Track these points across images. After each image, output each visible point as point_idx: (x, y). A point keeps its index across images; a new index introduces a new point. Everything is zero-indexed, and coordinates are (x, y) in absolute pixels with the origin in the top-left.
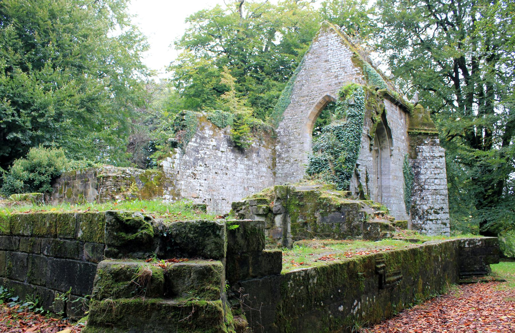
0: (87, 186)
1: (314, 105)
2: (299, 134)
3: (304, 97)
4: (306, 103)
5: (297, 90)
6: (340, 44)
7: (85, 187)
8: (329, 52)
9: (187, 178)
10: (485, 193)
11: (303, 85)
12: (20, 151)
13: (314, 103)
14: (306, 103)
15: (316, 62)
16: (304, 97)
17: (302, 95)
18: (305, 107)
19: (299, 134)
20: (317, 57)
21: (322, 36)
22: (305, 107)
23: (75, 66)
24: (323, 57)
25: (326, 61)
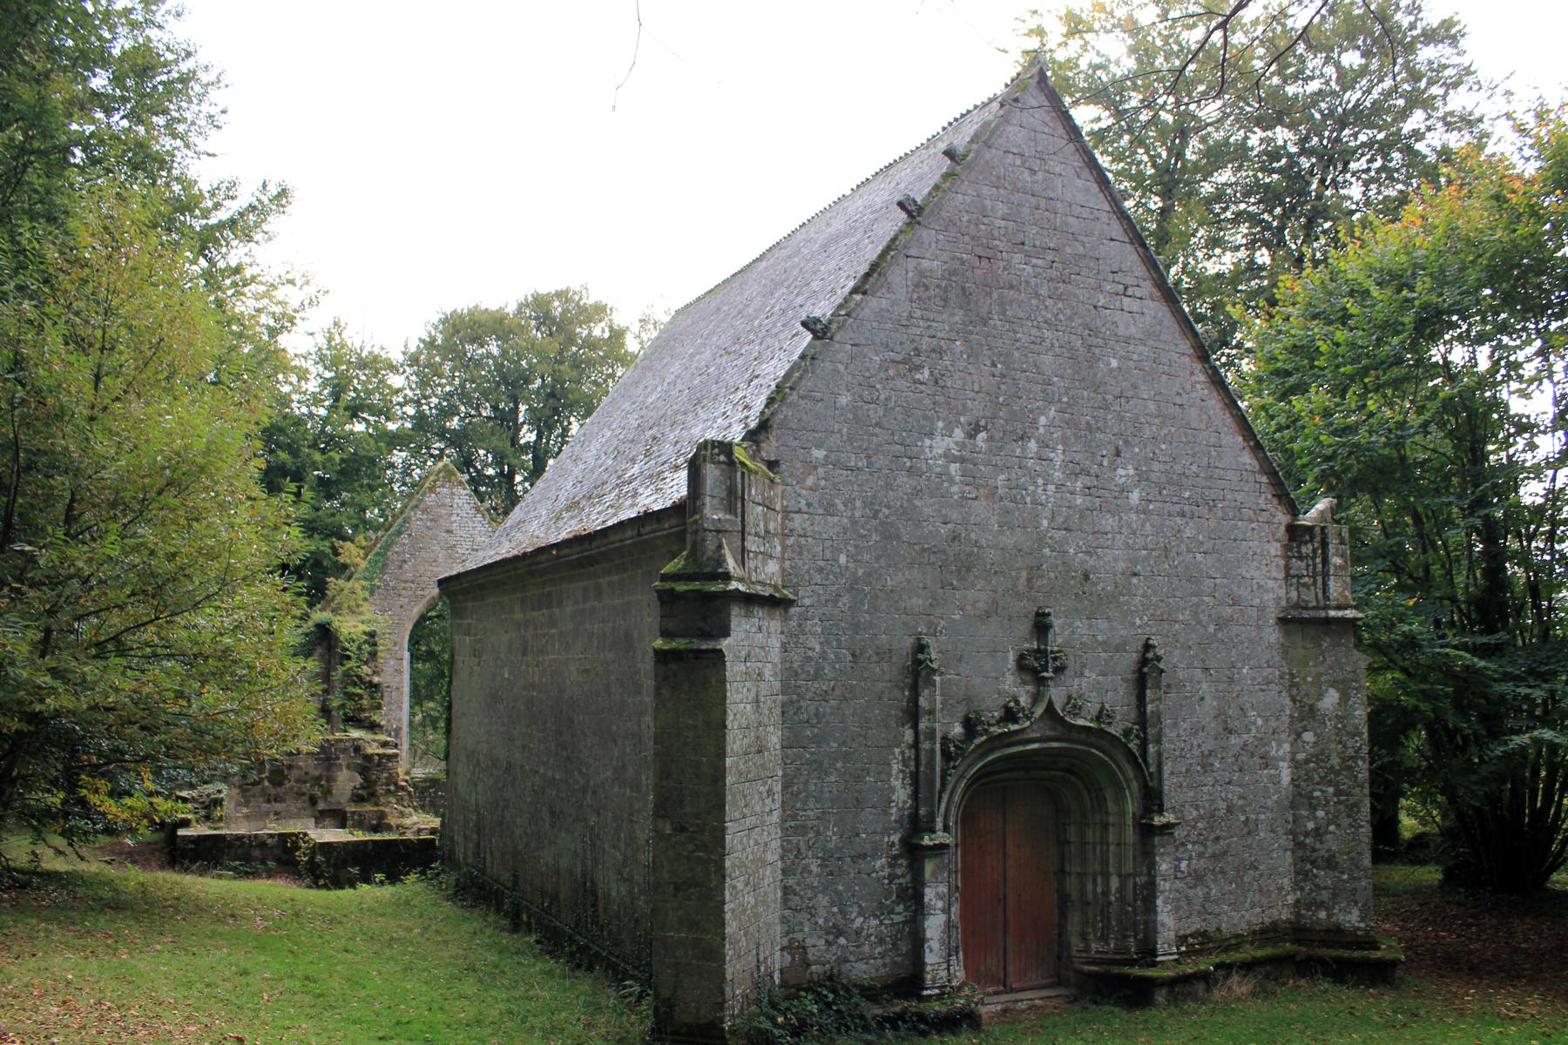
0: (334, 769)
1: (425, 601)
2: (395, 644)
3: (406, 582)
4: (410, 593)
5: (392, 568)
6: (473, 511)
7: (329, 768)
8: (454, 518)
9: (1463, 262)
10: (923, 482)
11: (405, 562)
12: (74, 156)
13: (423, 596)
14: (410, 593)
15: (429, 528)
16: (406, 582)
17: (403, 578)
18: (406, 600)
19: (395, 644)
20: (432, 520)
21: (443, 486)
22: (406, 600)
23: (915, 699)
24: (444, 523)
25: (448, 531)
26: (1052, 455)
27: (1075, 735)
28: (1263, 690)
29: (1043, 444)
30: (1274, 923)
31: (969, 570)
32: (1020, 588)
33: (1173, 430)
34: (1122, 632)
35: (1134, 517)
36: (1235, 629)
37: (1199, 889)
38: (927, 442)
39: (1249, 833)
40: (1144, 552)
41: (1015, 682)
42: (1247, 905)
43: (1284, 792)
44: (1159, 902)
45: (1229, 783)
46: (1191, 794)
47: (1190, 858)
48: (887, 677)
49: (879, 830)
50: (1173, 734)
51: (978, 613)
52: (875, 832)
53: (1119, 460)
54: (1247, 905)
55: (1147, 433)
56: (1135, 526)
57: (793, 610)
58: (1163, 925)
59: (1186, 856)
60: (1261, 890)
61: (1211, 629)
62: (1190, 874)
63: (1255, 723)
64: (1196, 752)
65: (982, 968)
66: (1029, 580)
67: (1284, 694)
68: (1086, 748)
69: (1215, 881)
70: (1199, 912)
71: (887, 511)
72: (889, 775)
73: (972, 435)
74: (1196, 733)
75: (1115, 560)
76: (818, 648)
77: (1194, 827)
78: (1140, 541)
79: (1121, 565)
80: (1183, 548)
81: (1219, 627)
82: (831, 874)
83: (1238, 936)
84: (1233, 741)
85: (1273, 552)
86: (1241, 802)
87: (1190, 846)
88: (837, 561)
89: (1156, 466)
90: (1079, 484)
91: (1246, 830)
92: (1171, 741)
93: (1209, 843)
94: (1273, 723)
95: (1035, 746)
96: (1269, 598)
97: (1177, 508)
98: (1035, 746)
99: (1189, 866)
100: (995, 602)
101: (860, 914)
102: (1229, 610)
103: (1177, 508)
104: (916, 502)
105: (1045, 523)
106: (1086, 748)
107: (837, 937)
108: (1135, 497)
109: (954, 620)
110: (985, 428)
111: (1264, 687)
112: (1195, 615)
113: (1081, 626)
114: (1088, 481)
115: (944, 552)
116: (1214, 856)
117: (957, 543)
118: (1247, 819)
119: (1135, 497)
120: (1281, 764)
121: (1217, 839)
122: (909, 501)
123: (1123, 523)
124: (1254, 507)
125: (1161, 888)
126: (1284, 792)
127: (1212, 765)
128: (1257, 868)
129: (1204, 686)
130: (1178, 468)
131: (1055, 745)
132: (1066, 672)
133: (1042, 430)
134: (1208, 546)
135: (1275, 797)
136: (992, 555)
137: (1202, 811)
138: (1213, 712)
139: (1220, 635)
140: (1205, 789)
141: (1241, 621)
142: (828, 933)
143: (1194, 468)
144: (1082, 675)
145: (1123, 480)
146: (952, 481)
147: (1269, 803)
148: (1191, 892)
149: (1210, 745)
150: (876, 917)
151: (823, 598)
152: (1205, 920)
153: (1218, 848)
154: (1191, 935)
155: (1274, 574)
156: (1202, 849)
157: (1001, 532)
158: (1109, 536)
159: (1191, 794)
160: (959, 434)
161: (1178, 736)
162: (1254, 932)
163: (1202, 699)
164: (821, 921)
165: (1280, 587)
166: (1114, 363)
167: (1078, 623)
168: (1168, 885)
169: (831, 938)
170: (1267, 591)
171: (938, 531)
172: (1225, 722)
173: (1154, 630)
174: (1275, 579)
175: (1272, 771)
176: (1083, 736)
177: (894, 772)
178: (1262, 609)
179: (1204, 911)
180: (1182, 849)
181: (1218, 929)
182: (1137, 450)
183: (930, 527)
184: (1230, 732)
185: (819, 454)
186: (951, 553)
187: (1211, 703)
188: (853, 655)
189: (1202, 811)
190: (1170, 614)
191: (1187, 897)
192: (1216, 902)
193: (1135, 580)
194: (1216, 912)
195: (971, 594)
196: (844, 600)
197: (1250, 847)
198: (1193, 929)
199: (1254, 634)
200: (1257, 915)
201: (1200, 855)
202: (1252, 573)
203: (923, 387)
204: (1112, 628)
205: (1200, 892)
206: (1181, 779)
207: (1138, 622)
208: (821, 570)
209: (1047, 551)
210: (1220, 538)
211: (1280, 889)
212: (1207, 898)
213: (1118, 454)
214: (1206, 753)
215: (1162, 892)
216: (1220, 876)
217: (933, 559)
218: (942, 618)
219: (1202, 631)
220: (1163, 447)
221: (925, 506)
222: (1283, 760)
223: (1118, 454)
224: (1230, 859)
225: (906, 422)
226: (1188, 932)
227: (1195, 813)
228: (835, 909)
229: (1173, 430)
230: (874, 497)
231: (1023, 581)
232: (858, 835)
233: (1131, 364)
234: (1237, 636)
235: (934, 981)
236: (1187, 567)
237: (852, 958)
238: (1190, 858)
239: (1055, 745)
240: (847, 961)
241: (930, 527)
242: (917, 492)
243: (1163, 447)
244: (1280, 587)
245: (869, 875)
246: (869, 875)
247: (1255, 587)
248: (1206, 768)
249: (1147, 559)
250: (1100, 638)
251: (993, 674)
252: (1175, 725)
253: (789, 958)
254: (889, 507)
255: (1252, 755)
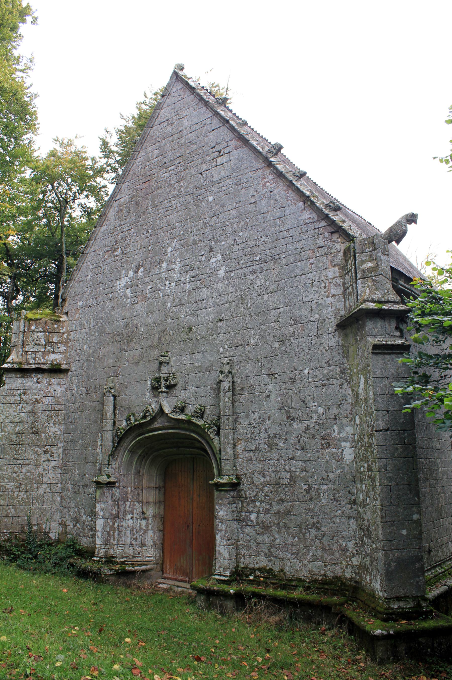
26: (174, 266)
27: (182, 425)
28: (325, 385)
29: (170, 262)
30: (337, 578)
31: (132, 340)
32: (155, 344)
33: (248, 220)
34: (211, 359)
35: (221, 284)
36: (295, 343)
37: (265, 536)
38: (118, 282)
39: (311, 499)
40: (227, 304)
41: (150, 396)
42: (309, 557)
43: (347, 468)
44: (218, 537)
45: (291, 459)
46: (260, 465)
47: (258, 512)
48: (97, 399)
49: (92, 474)
50: (246, 423)
51: (134, 361)
52: (91, 475)
53: (212, 254)
54: (309, 557)
55: (230, 229)
56: (221, 290)
57: (70, 373)
58: (220, 554)
59: (255, 510)
60: (323, 548)
61: (276, 345)
62: (258, 524)
63: (316, 412)
64: (263, 435)
65: (178, 564)
66: (159, 338)
67: (345, 386)
68: (188, 433)
69: (279, 532)
70: (266, 554)
71: (101, 321)
72: (97, 447)
73: (136, 272)
74: (264, 421)
75: (208, 315)
76: (76, 388)
77: (262, 490)
78: (224, 299)
79: (212, 316)
80: (255, 293)
81: (282, 342)
82: (75, 493)
83: (300, 580)
84: (296, 426)
85: (331, 275)
86: (303, 474)
87: (258, 504)
88: (83, 349)
89: (236, 248)
90: (188, 276)
91: (308, 496)
92: (244, 427)
93: (274, 503)
94: (334, 411)
95: (160, 432)
96: (328, 312)
97: (251, 269)
98: (160, 432)
99: (257, 517)
100: (142, 354)
101: (85, 514)
102: (291, 329)
103: (251, 269)
104: (113, 313)
105: (169, 305)
106: (188, 433)
107: (77, 523)
108: (221, 273)
109: (125, 367)
110: (142, 266)
111: (325, 382)
112: (263, 337)
113: (186, 359)
114: (192, 273)
115: (122, 334)
116: (278, 513)
117: (128, 328)
118: (309, 488)
119: (221, 273)
120: (343, 444)
121: (282, 501)
122: (110, 313)
123: (214, 290)
124: (313, 247)
125: (220, 528)
126: (347, 468)
127: (276, 444)
128: (319, 529)
129: (270, 387)
130: (251, 243)
131: (170, 431)
132: (177, 388)
133: (169, 255)
134: (273, 287)
135: (338, 472)
136: (142, 330)
137: (268, 478)
138: (277, 406)
139: (283, 348)
140: (271, 462)
141: (301, 334)
142: (74, 521)
143: (263, 239)
144: (186, 388)
145: (214, 264)
146: (127, 298)
147: (331, 476)
148: (259, 538)
149: (275, 430)
150: (90, 517)
151: (78, 366)
152: (270, 561)
153: (282, 508)
154: (259, 569)
155: (333, 292)
156: (268, 507)
157: (147, 317)
158: (205, 301)
159: (260, 465)
160: (131, 273)
161: (250, 423)
162: (315, 581)
163: (268, 396)
164: (72, 514)
165: (339, 301)
166: (211, 198)
167: (185, 358)
168: (224, 527)
169: (75, 523)
170: (326, 307)
171: (120, 324)
172: (288, 412)
173: (232, 354)
174: (334, 295)
175: (335, 450)
176: (186, 426)
177: (98, 445)
178: (321, 322)
179: (269, 555)
180: (251, 505)
181: (282, 570)
182: (223, 243)
183: (117, 323)
184: (293, 420)
185: (80, 304)
186: (125, 334)
187: (275, 399)
188: (87, 390)
189: (268, 478)
190: (244, 341)
191: (256, 541)
192: (280, 548)
193: (220, 324)
194: (281, 556)
195: (132, 353)
196: (85, 366)
197: (312, 510)
198: (261, 565)
199: (314, 342)
200: (319, 567)
201: (267, 512)
202: (312, 296)
203: (117, 258)
204: (204, 357)
205: (266, 538)
206: (252, 454)
207: (221, 350)
208: (78, 354)
209: (169, 320)
210: (282, 279)
211: (345, 550)
212: (272, 544)
213: (211, 250)
214: (272, 435)
215: (220, 531)
216: (284, 530)
217: (117, 338)
218: (120, 367)
219: (269, 348)
220: (241, 234)
221: (116, 314)
222: (346, 441)
223: (211, 250)
224: (292, 517)
225: (111, 277)
226: (257, 566)
227: (262, 479)
228: (76, 510)
229: (248, 220)
230: (97, 316)
231: (156, 340)
232: (85, 475)
233: (221, 194)
234: (298, 346)
235: (98, 553)
236: (257, 306)
237: (81, 535)
238: (258, 512)
239: (170, 431)
240: (79, 536)
241: (117, 323)
242: (113, 308)
243: (241, 234)
244: (339, 301)
245: (88, 495)
246: (88, 495)
247: (314, 307)
248: (272, 446)
249: (229, 308)
250: (196, 365)
251: (141, 393)
252: (247, 416)
253: (61, 529)
254: (102, 319)
255: (314, 437)
